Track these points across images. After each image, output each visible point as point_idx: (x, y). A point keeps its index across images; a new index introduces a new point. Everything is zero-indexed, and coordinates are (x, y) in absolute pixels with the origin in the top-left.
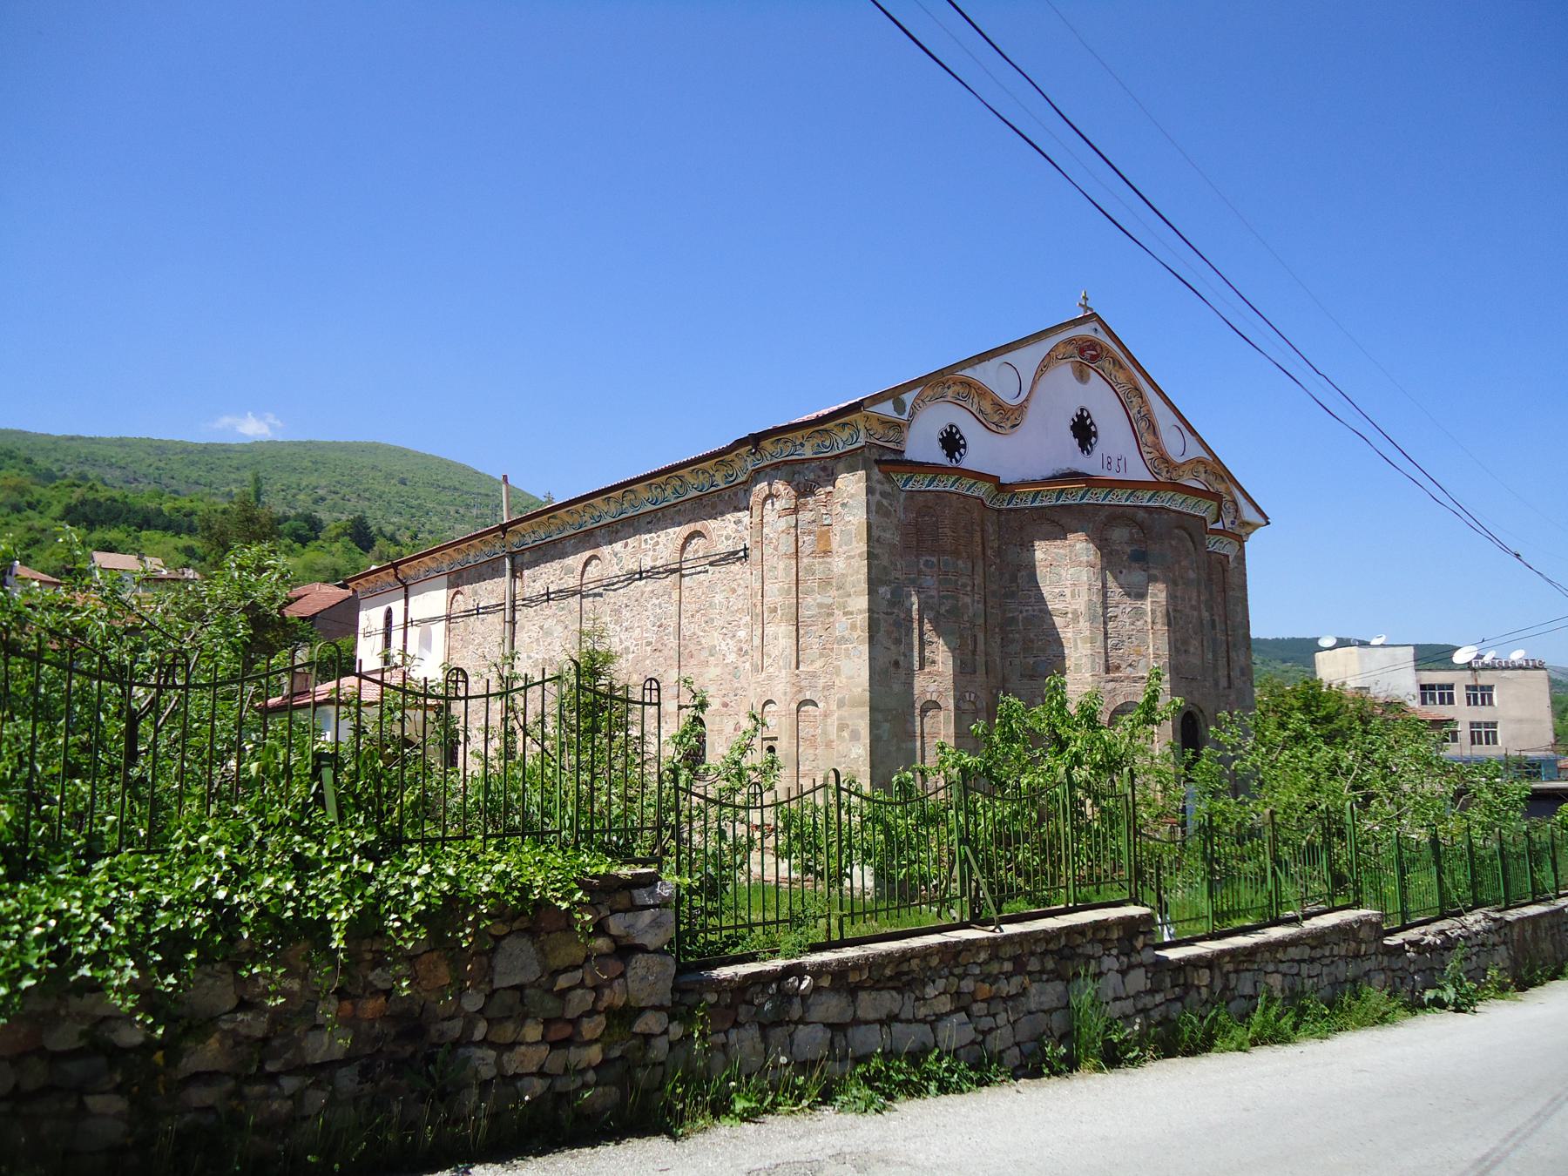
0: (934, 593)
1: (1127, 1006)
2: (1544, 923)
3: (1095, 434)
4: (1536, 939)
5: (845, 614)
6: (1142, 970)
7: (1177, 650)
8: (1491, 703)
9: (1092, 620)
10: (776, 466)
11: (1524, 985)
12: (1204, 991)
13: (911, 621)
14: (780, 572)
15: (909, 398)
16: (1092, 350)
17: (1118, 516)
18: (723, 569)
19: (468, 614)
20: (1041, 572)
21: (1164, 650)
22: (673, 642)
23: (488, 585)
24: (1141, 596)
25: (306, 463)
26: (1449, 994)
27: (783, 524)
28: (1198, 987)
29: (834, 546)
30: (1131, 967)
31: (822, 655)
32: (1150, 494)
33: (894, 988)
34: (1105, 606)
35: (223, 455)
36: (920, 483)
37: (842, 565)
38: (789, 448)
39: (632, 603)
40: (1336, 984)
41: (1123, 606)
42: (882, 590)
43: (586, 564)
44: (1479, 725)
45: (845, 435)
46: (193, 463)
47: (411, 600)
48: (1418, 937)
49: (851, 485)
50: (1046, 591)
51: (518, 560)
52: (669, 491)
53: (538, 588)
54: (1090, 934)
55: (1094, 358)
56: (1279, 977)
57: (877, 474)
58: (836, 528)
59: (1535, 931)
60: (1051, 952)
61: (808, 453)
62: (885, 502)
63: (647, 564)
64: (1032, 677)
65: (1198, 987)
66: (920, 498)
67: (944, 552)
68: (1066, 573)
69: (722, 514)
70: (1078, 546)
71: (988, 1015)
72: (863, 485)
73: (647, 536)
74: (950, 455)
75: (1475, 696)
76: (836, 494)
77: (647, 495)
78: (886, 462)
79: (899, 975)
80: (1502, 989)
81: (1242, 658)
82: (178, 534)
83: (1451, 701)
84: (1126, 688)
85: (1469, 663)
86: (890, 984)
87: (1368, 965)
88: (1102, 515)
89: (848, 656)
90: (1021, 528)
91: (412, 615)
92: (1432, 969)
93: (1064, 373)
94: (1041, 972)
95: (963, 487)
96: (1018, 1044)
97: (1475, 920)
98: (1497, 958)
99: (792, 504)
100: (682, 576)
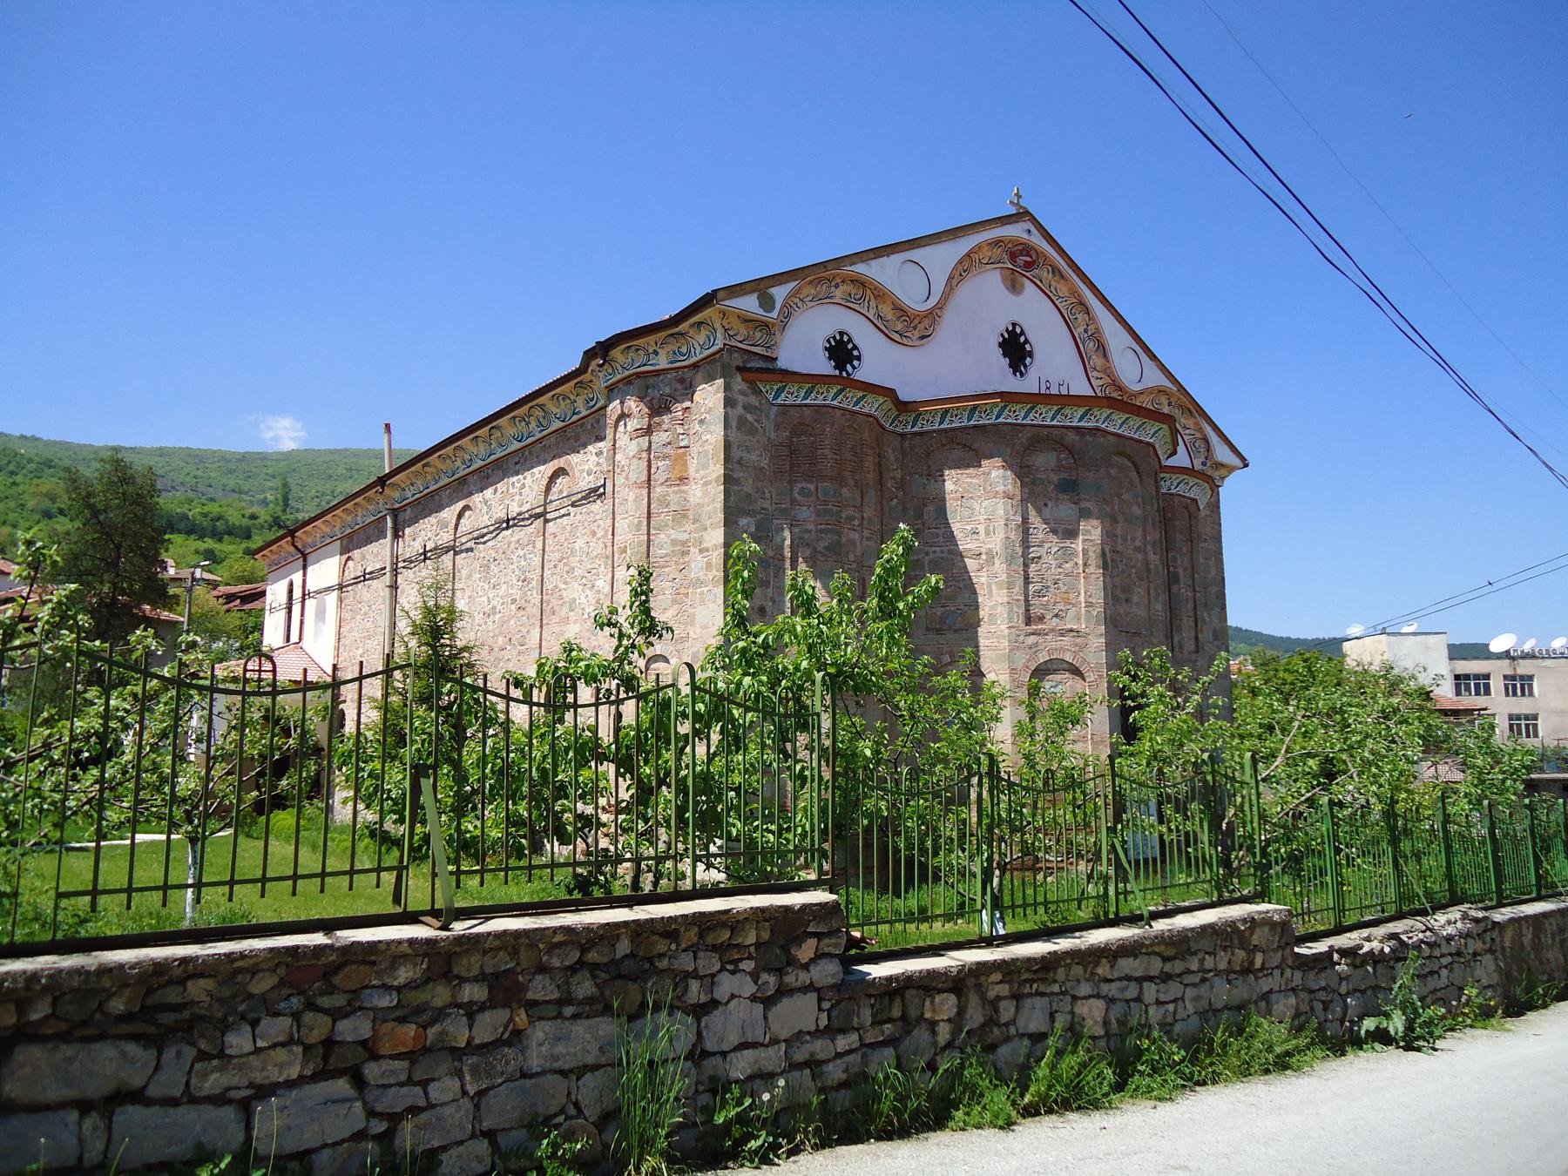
0: (811, 526)
1: (772, 1058)
2: (1551, 926)
3: (1030, 354)
4: (1537, 945)
5: (701, 551)
6: (812, 997)
7: (1116, 599)
8: (1531, 694)
9: (1010, 561)
10: (628, 381)
11: (1516, 1007)
12: (944, 1032)
13: (783, 559)
14: (629, 499)
15: (780, 293)
16: (1025, 258)
17: (1041, 439)
18: (584, 509)
19: (358, 580)
20: (951, 505)
21: (1099, 598)
22: (535, 598)
23: (373, 548)
24: (1072, 534)
25: (341, 470)
26: (1397, 1024)
27: (633, 447)
28: (933, 1024)
29: (692, 472)
30: (783, 992)
31: (674, 602)
32: (1081, 411)
33: (134, 1037)
34: (1026, 545)
35: (259, 463)
36: (794, 396)
37: (698, 493)
38: (642, 358)
39: (500, 556)
40: (1209, 1013)
41: (1048, 547)
42: (743, 522)
43: (460, 516)
44: (1518, 717)
45: (702, 338)
46: (231, 472)
47: (310, 569)
48: (1351, 944)
49: (709, 397)
50: (956, 528)
51: (401, 518)
52: (533, 425)
53: (417, 547)
54: (692, 935)
55: (1029, 266)
56: (1099, 1004)
57: (739, 383)
58: (694, 450)
59: (1536, 935)
60: (594, 967)
61: (662, 362)
62: (750, 417)
63: (514, 510)
64: (938, 631)
65: (933, 1024)
66: (795, 414)
67: (822, 478)
68: (981, 506)
69: (585, 446)
70: (994, 474)
71: (409, 1082)
72: (721, 395)
73: (515, 479)
74: (840, 366)
75: (1514, 686)
76: (694, 410)
77: (512, 431)
78: (751, 369)
79: (148, 1012)
80: (1485, 1015)
81: (1216, 620)
82: (201, 538)
83: (1487, 692)
84: (1051, 642)
85: (1508, 652)
86: (125, 1029)
87: (1265, 984)
88: (1023, 438)
89: (703, 602)
90: (928, 455)
91: (311, 587)
92: (1376, 988)
93: (989, 283)
94: (560, 1003)
95: (849, 400)
96: (490, 1135)
97: (1448, 921)
98: (1479, 972)
99: (644, 423)
100: (547, 521)
